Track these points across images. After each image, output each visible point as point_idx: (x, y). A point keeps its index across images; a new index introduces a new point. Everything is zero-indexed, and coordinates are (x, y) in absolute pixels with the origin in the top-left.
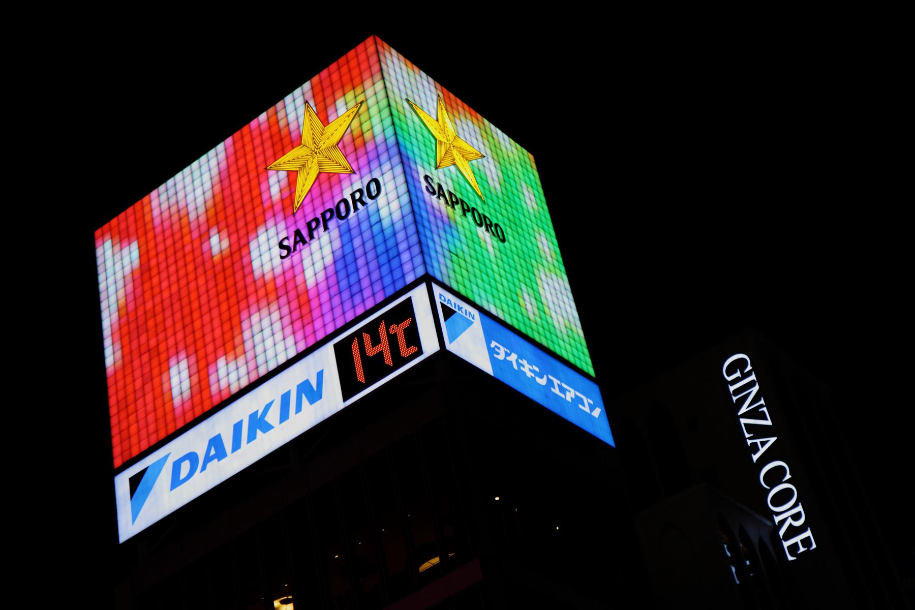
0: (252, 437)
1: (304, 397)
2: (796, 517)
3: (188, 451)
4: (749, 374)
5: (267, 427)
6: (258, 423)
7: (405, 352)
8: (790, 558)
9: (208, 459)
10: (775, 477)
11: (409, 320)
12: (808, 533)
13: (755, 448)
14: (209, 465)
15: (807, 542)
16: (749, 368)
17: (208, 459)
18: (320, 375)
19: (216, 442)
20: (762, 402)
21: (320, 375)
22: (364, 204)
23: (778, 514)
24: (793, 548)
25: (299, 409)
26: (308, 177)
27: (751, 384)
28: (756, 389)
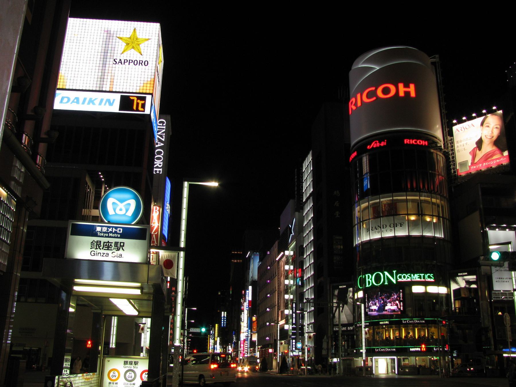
0: (89, 104)
1: (107, 102)
2: (160, 165)
3: (69, 97)
4: (164, 126)
5: (94, 104)
6: (91, 101)
7: (140, 109)
8: (154, 173)
9: (73, 102)
10: (159, 153)
11: (144, 102)
12: (161, 170)
13: (157, 144)
14: (73, 103)
15: (160, 171)
16: (165, 125)
17: (73, 102)
18: (114, 100)
19: (77, 99)
20: (164, 134)
21: (114, 100)
22: (142, 65)
23: (156, 162)
24: (156, 171)
25: (105, 104)
26: (128, 49)
27: (163, 129)
28: (164, 130)
